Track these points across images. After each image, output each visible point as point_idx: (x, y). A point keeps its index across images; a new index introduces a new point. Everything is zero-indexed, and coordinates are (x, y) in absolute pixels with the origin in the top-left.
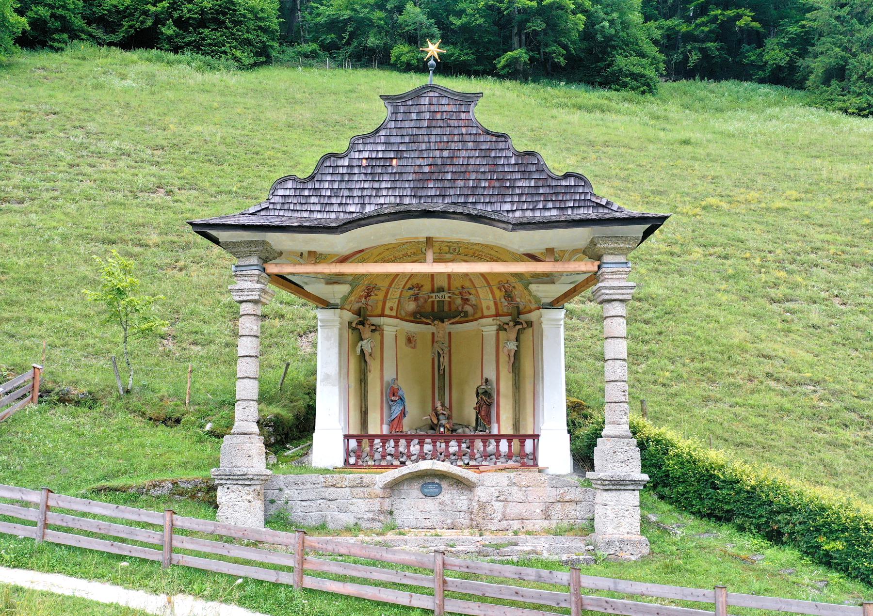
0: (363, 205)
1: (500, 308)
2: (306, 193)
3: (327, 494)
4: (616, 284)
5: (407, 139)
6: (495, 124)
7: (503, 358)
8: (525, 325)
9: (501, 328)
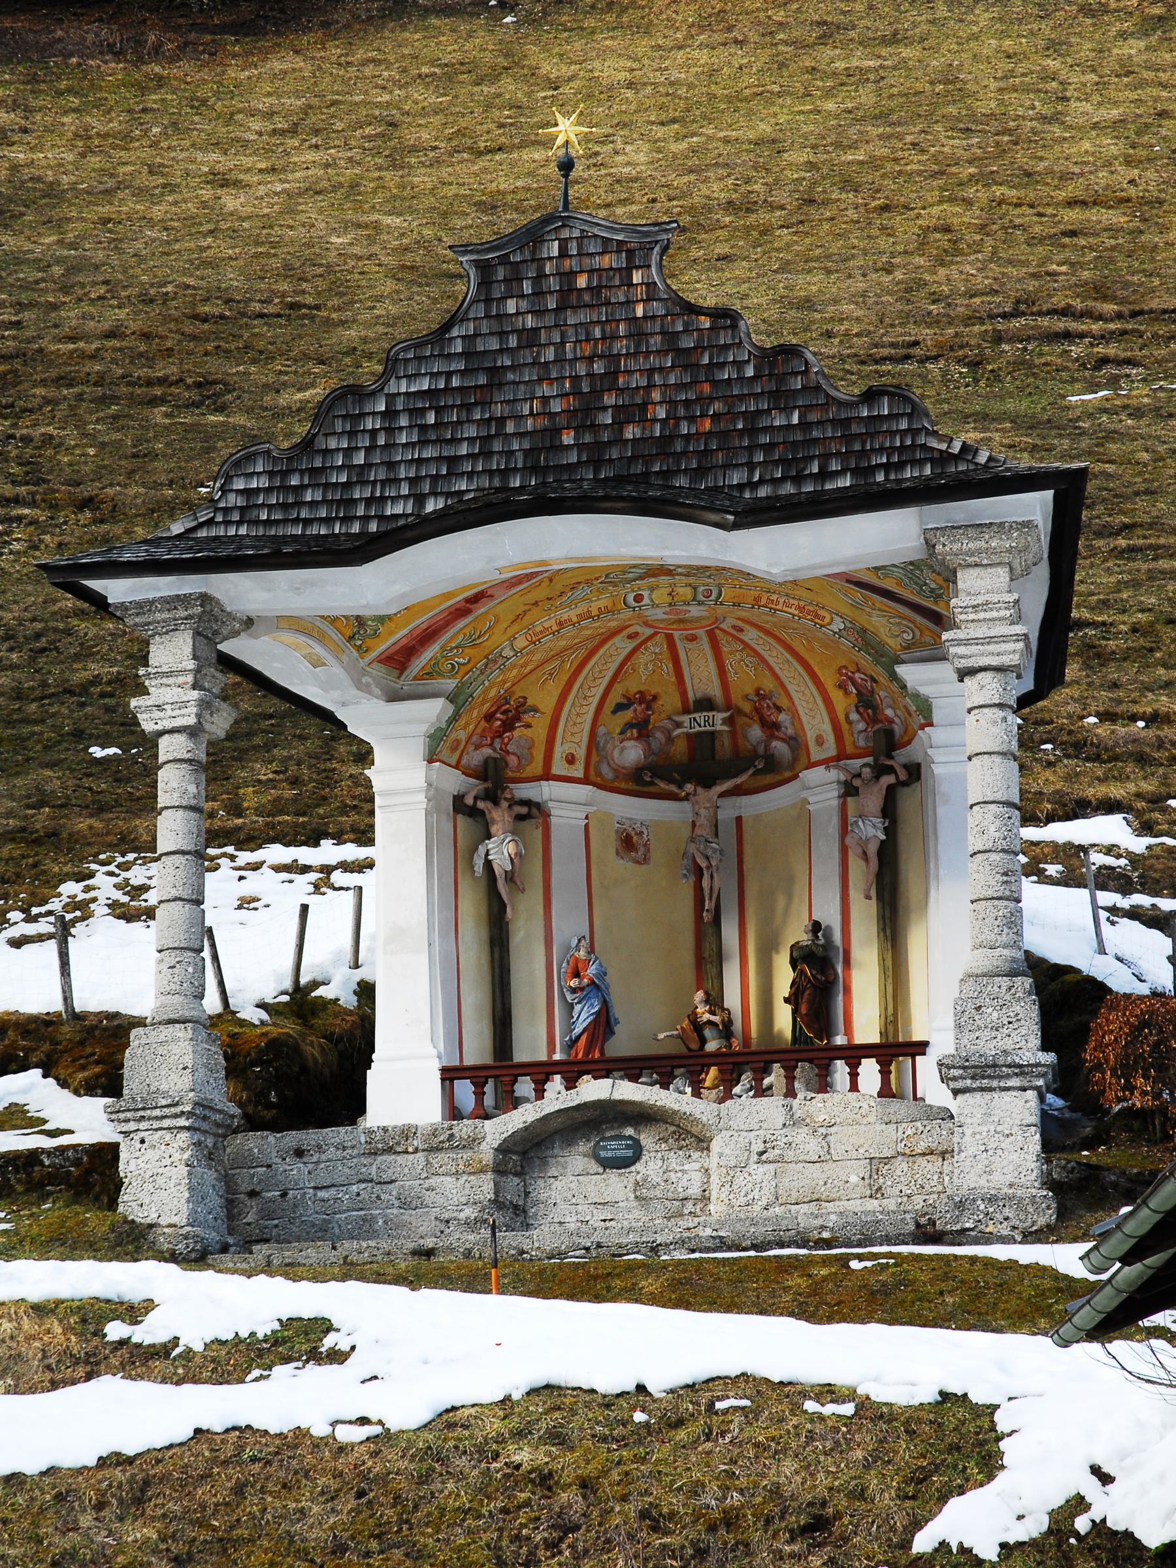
0: (420, 500)
1: (848, 740)
2: (294, 481)
4: (980, 632)
6: (705, 292)
7: (856, 866)
8: (903, 776)
9: (849, 790)
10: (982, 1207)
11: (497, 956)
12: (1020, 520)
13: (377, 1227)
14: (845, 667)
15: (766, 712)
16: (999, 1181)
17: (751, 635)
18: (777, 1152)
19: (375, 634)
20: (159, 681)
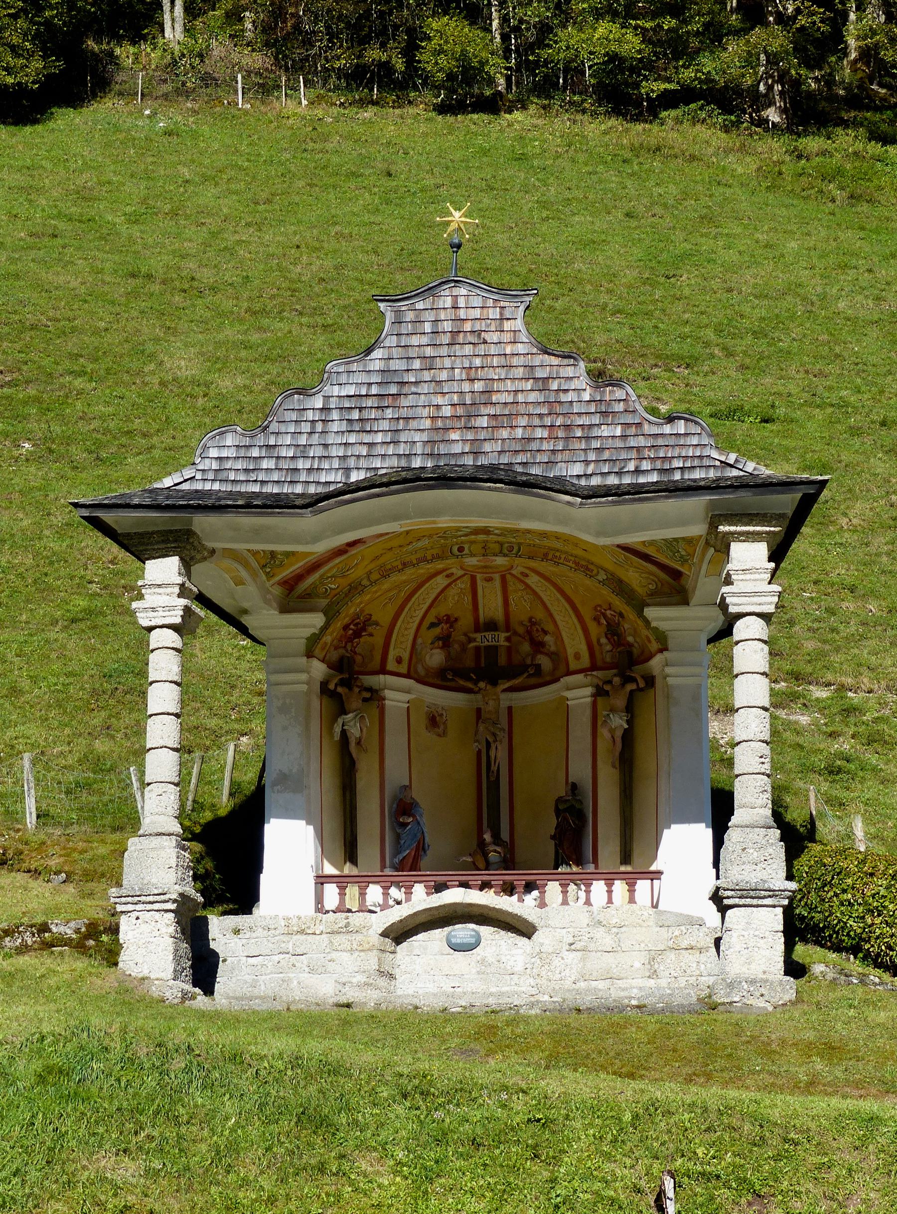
0: (347, 471)
1: (597, 654)
2: (255, 453)
3: (290, 945)
5: (417, 364)
8: (642, 684)
9: (600, 692)
10: (746, 987)
11: (348, 798)
12: (778, 512)
13: (292, 986)
14: (600, 606)
15: (535, 634)
16: (755, 970)
17: (533, 580)
18: (582, 943)
19: (281, 565)
20: (153, 590)
